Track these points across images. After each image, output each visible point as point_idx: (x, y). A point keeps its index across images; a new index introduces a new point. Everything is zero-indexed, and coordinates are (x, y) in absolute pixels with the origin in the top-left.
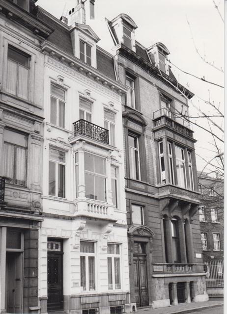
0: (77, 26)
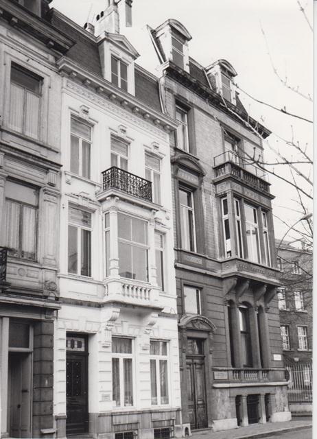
0: (108, 36)
